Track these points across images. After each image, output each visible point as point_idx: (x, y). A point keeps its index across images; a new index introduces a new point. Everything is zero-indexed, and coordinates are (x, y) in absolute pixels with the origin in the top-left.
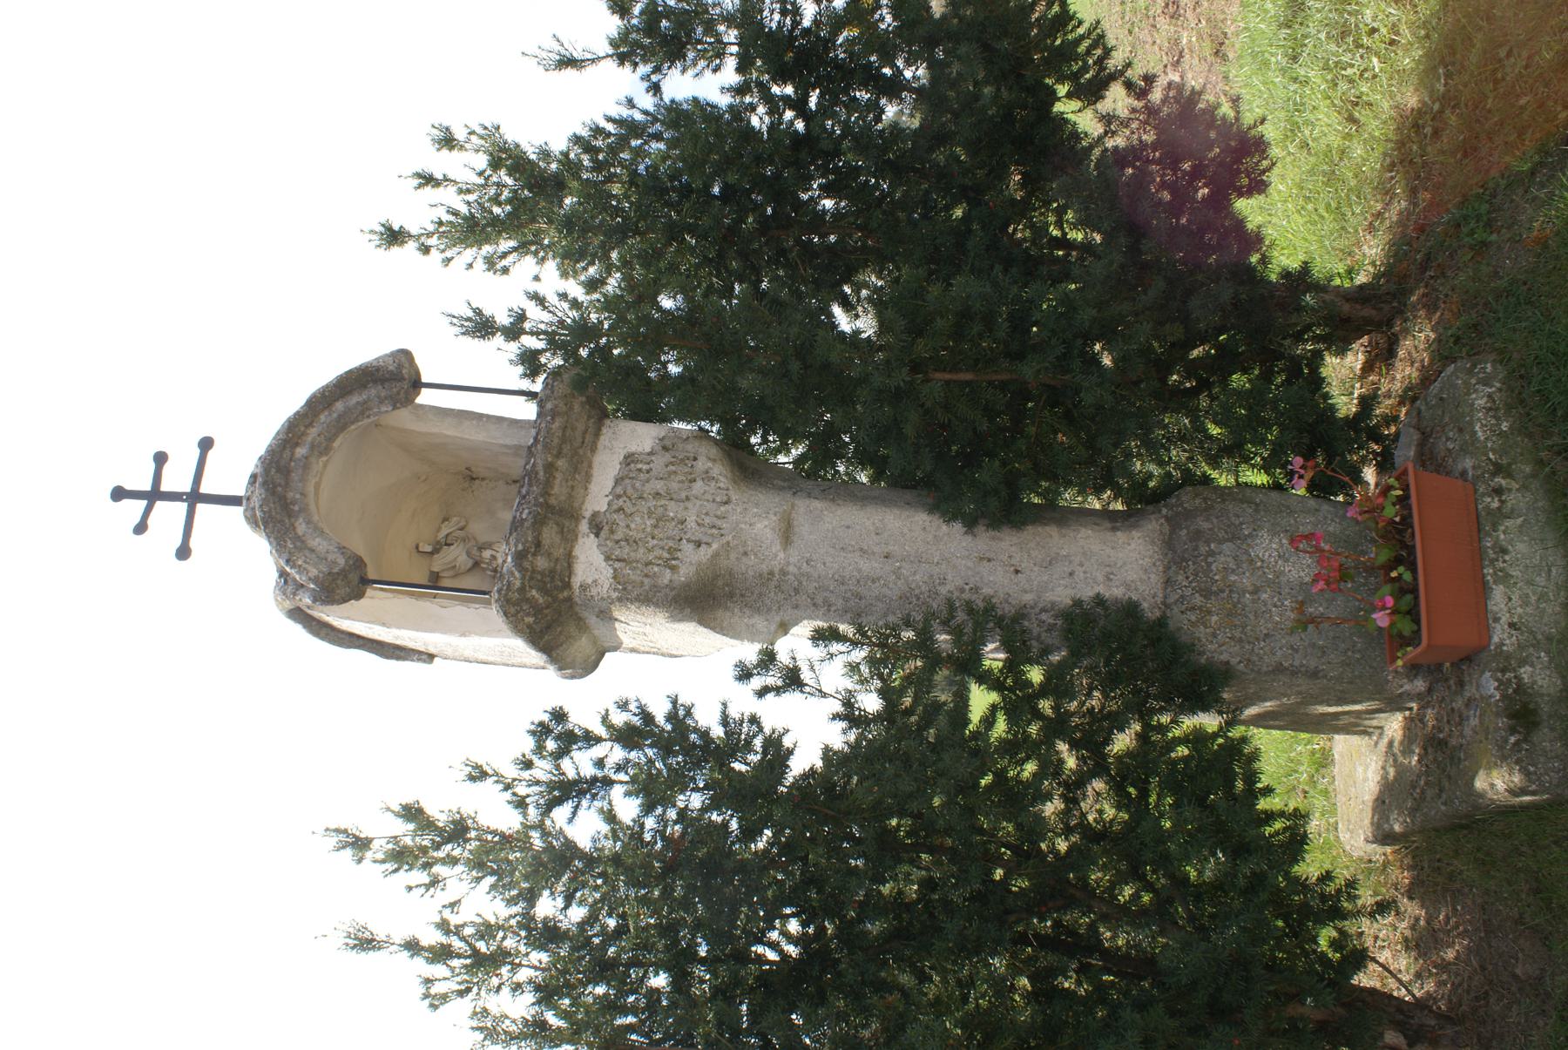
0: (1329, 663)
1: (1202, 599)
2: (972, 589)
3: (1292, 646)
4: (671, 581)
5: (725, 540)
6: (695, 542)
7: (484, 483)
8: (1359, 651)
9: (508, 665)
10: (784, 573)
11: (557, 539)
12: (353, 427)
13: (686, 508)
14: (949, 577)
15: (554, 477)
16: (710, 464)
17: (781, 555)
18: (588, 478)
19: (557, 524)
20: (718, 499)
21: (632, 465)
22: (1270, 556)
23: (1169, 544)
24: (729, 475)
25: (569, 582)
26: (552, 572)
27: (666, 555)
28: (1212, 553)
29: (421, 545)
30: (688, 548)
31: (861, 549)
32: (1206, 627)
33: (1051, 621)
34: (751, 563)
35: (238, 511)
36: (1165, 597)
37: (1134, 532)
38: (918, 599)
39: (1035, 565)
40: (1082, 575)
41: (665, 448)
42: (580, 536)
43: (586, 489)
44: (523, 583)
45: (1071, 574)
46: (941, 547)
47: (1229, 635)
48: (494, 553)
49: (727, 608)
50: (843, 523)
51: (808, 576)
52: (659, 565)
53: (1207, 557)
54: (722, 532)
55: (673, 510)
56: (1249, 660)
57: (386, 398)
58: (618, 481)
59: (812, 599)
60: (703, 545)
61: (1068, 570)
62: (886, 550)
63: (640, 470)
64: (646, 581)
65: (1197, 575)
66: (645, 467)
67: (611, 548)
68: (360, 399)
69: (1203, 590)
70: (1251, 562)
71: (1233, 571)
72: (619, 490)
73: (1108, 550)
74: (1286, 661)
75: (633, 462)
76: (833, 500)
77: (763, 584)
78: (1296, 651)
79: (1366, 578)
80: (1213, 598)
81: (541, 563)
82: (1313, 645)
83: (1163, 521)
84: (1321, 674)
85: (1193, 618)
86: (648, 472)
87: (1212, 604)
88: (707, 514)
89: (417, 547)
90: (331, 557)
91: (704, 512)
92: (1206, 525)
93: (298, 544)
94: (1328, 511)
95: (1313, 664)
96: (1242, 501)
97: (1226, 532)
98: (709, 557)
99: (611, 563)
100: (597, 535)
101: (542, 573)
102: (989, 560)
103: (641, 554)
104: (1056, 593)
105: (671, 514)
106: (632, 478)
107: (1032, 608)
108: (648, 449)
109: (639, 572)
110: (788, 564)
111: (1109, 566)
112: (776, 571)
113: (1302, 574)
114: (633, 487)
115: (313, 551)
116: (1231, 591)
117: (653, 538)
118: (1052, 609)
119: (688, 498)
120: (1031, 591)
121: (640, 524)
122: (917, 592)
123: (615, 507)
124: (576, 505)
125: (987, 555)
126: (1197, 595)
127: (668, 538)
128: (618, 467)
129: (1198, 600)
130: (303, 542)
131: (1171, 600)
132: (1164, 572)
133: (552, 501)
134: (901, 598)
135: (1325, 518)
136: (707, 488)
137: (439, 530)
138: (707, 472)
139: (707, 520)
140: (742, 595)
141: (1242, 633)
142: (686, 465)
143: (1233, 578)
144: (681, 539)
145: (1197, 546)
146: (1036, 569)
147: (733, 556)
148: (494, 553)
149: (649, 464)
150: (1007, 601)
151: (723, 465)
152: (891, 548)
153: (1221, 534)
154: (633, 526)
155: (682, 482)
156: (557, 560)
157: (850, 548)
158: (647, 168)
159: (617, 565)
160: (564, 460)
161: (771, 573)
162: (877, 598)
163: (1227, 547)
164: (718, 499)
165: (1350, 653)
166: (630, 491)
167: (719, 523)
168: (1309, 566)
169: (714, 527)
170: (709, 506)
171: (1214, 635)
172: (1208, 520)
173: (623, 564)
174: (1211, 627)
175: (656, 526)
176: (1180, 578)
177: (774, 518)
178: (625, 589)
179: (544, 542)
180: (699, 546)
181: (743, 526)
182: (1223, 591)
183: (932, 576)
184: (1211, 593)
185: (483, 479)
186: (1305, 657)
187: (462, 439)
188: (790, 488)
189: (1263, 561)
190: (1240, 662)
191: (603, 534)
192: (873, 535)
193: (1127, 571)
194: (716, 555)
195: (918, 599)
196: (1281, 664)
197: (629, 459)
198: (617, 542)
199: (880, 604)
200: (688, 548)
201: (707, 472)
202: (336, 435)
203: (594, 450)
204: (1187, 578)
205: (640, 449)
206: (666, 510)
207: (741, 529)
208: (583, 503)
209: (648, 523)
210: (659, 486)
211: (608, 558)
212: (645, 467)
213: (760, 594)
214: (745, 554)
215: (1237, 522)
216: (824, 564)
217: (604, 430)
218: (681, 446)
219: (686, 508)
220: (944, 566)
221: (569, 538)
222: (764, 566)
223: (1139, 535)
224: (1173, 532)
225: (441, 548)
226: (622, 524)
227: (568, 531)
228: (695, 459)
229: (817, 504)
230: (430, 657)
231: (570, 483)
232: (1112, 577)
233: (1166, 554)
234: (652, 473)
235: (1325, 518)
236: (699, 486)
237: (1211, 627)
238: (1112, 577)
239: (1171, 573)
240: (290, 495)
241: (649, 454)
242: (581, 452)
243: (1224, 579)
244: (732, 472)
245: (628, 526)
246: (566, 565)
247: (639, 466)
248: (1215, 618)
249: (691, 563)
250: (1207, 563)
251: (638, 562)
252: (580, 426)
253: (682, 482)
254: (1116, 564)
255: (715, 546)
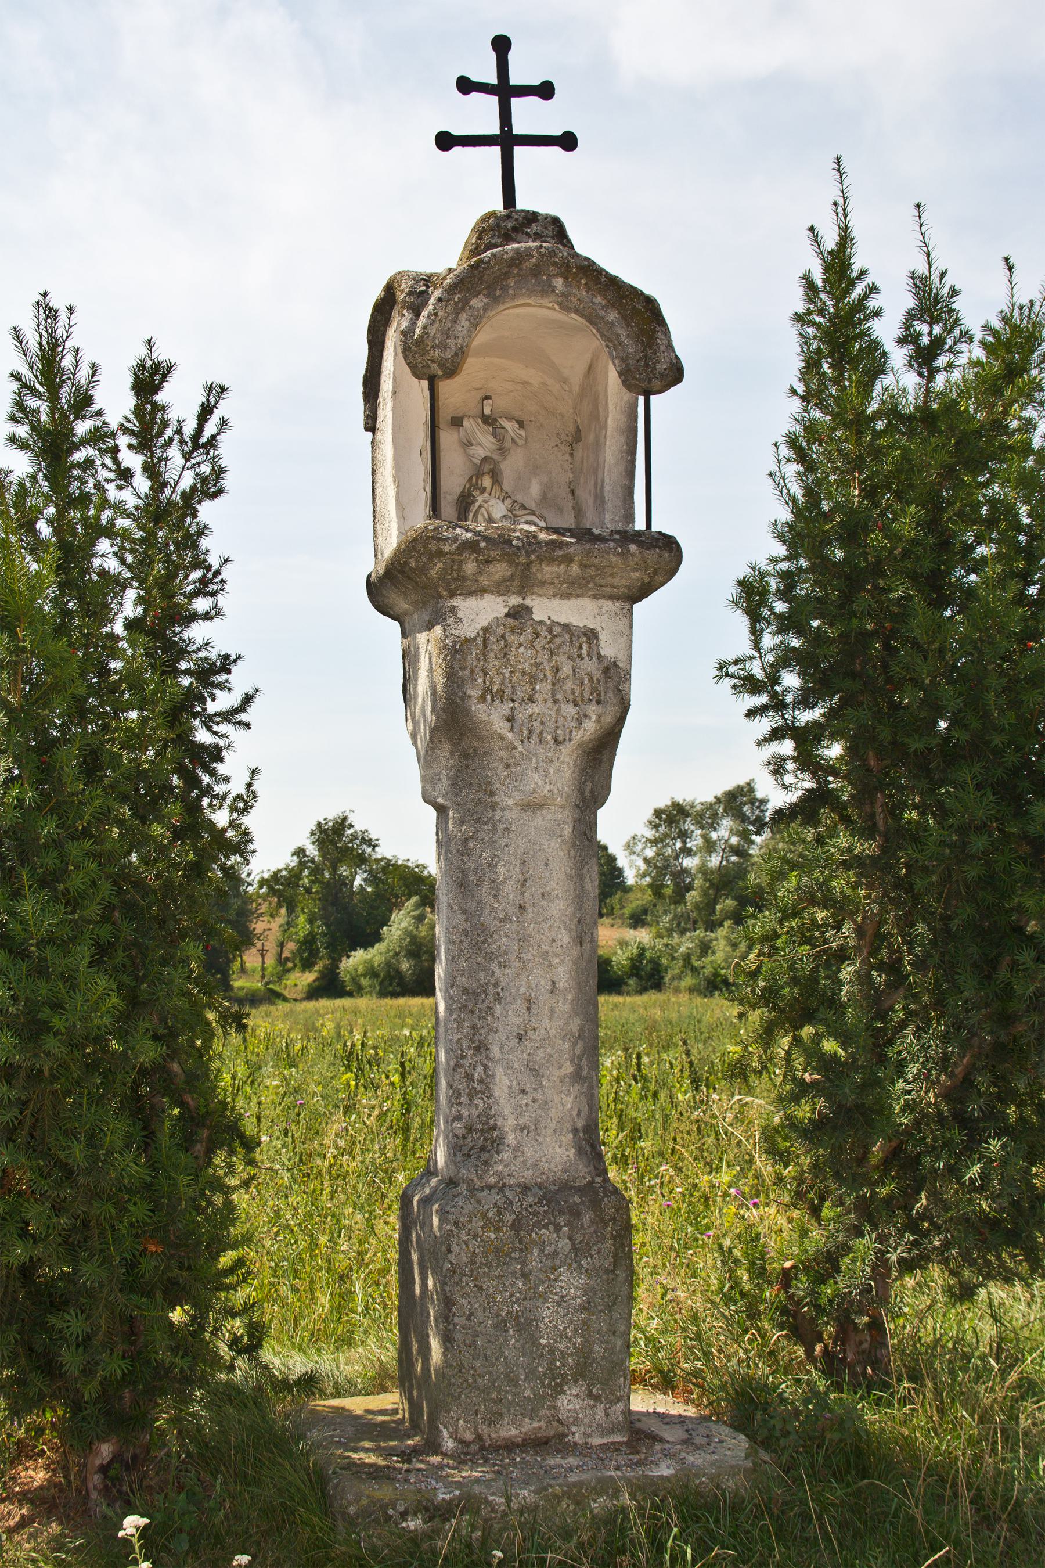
0: (460, 1352)
1: (510, 1222)
2: (498, 994)
3: (473, 1314)
4: (470, 697)
5: (518, 744)
6: (513, 716)
7: (567, 457)
8: (475, 1381)
9: (374, 516)
10: (494, 806)
11: (497, 577)
12: (594, 331)
13: (545, 701)
14: (507, 971)
15: (559, 565)
16: (594, 718)
17: (510, 802)
18: (566, 596)
19: (512, 575)
20: (559, 732)
21: (584, 639)
22: (562, 1287)
23: (565, 1187)
24: (586, 738)
25: (456, 595)
26: (464, 578)
27: (495, 688)
28: (558, 1228)
29: (490, 401)
30: (506, 708)
31: (525, 881)
32: (482, 1228)
33: (476, 1077)
34: (499, 772)
35: (497, 204)
36: (510, 1186)
37: (573, 1150)
38: (483, 942)
39: (529, 1054)
40: (524, 1102)
41: (606, 670)
42: (504, 598)
43: (554, 596)
44: (447, 553)
45: (523, 1091)
46: (537, 959)
47: (477, 1250)
48: (488, 490)
49: (452, 753)
50: (550, 858)
51: (494, 830)
52: (484, 682)
53: (554, 1224)
54: (526, 741)
55: (543, 688)
56: (454, 1273)
57: (627, 365)
58: (566, 627)
59: (472, 837)
60: (509, 724)
61: (527, 1088)
62: (527, 906)
63: (581, 647)
64: (467, 672)
65: (534, 1215)
66: (584, 652)
67: (495, 632)
68: (623, 338)
69: (519, 1222)
70: (554, 1269)
71: (542, 1251)
72: (557, 630)
73: (552, 1126)
74: (457, 1309)
75: (589, 638)
76: (574, 845)
77: (480, 786)
78: (468, 1319)
79: (549, 1385)
80: (513, 1232)
81: (470, 567)
82: (476, 1335)
83: (589, 1179)
84: (448, 1344)
85: (490, 1214)
86: (580, 656)
87: (507, 1232)
88: (543, 723)
89: (487, 398)
90: (451, 342)
91: (544, 720)
92: (586, 1220)
93: (460, 305)
94: (615, 1345)
95: (458, 1336)
96: (615, 1256)
97: (581, 1242)
98: (499, 731)
99: (481, 634)
100: (507, 615)
101: (460, 569)
102: (529, 1009)
103: (494, 662)
104: (503, 1078)
105: (538, 687)
106: (571, 642)
107: (487, 1056)
108: (603, 653)
109: (475, 664)
110: (503, 810)
111: (536, 1128)
112: (497, 799)
113: (547, 1320)
114: (564, 643)
115: (455, 322)
116: (521, 1250)
117: (511, 672)
118: (488, 1076)
119: (556, 701)
120: (502, 1053)
121: (524, 657)
122: (490, 940)
123: (539, 629)
124: (536, 589)
125: (533, 1006)
126: (514, 1217)
127: (513, 687)
128: (582, 625)
129: (509, 1218)
130: (463, 309)
131: (508, 1193)
132: (536, 1184)
133: (534, 568)
134: (483, 925)
135: (607, 1342)
136: (569, 719)
137: (510, 418)
138: (586, 716)
139: (536, 724)
140: (467, 767)
141: (481, 1263)
142: (591, 694)
143: (535, 1252)
144: (513, 701)
145: (564, 1214)
146: (525, 1055)
147: (503, 754)
148: (488, 490)
149: (588, 655)
150: (490, 1030)
151: (596, 731)
152: (530, 910)
153: (579, 1237)
154: (521, 650)
155: (573, 693)
156: (476, 581)
157: (525, 869)
158: (1029, 516)
159: (479, 640)
160: (579, 570)
161: (492, 794)
162: (479, 902)
163: (565, 1245)
164: (559, 732)
165: (472, 1372)
166: (558, 641)
167: (534, 737)
168: (556, 1327)
169: (530, 732)
170: (550, 726)
171: (475, 1236)
172: (592, 1222)
173: (481, 647)
174: (484, 1232)
175: (524, 673)
176: (531, 1199)
177: (546, 791)
178: (456, 652)
179: (491, 566)
180: (509, 720)
181: (534, 761)
182: (521, 1242)
183: (506, 954)
184: (518, 1231)
185: (572, 455)
186: (464, 1328)
187: (605, 437)
188: (583, 800)
189: (555, 1280)
190: (451, 1263)
191: (510, 622)
192: (542, 890)
193: (533, 1146)
194: (502, 738)
195: (483, 942)
196: (454, 1304)
197: (591, 635)
198: (503, 637)
199: (474, 904)
200: (506, 708)
201: (586, 716)
202: (582, 316)
203: (595, 597)
204: (531, 1206)
205: (602, 644)
206: (542, 681)
207: (531, 759)
208: (539, 595)
209: (526, 665)
210: (566, 670)
211: (485, 630)
212: (584, 652)
213: (470, 784)
214: (508, 766)
215: (593, 1253)
216: (507, 846)
217: (618, 604)
218: (611, 684)
219: (545, 701)
220: (517, 964)
221: (501, 588)
222: (498, 785)
223: (572, 1156)
224: (579, 1190)
225: (490, 425)
226: (522, 639)
227: (507, 587)
228: (598, 702)
229: (568, 830)
230: (371, 425)
231: (557, 581)
232: (526, 1132)
233: (554, 1184)
234: (578, 660)
235: (607, 1342)
236: (570, 710)
237: (484, 1232)
238: (526, 1132)
239: (536, 1190)
240: (511, 282)
241: (599, 654)
242: (591, 585)
243: (534, 1243)
244: (591, 740)
245: (521, 645)
246: (473, 588)
247: (585, 647)
248: (493, 1236)
249: (490, 715)
250: (547, 1224)
251: (485, 660)
252: (617, 581)
253: (573, 693)
254: (539, 1135)
255: (510, 736)
